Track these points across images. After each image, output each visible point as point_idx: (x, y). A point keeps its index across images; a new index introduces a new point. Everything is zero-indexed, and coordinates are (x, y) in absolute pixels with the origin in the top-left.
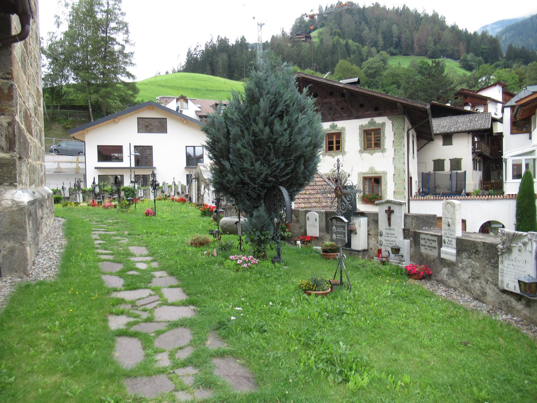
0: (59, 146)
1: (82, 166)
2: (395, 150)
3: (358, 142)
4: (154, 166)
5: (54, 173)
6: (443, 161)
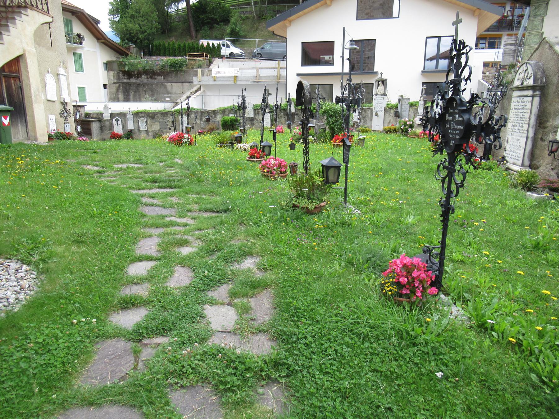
0: (262, 48)
1: (283, 72)
4: (375, 70)
5: (252, 83)
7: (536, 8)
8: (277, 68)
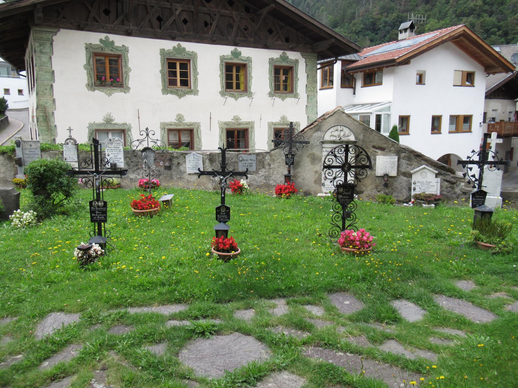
2: (308, 96)
3: (268, 81)
6: (236, 89)
7: (40, 45)
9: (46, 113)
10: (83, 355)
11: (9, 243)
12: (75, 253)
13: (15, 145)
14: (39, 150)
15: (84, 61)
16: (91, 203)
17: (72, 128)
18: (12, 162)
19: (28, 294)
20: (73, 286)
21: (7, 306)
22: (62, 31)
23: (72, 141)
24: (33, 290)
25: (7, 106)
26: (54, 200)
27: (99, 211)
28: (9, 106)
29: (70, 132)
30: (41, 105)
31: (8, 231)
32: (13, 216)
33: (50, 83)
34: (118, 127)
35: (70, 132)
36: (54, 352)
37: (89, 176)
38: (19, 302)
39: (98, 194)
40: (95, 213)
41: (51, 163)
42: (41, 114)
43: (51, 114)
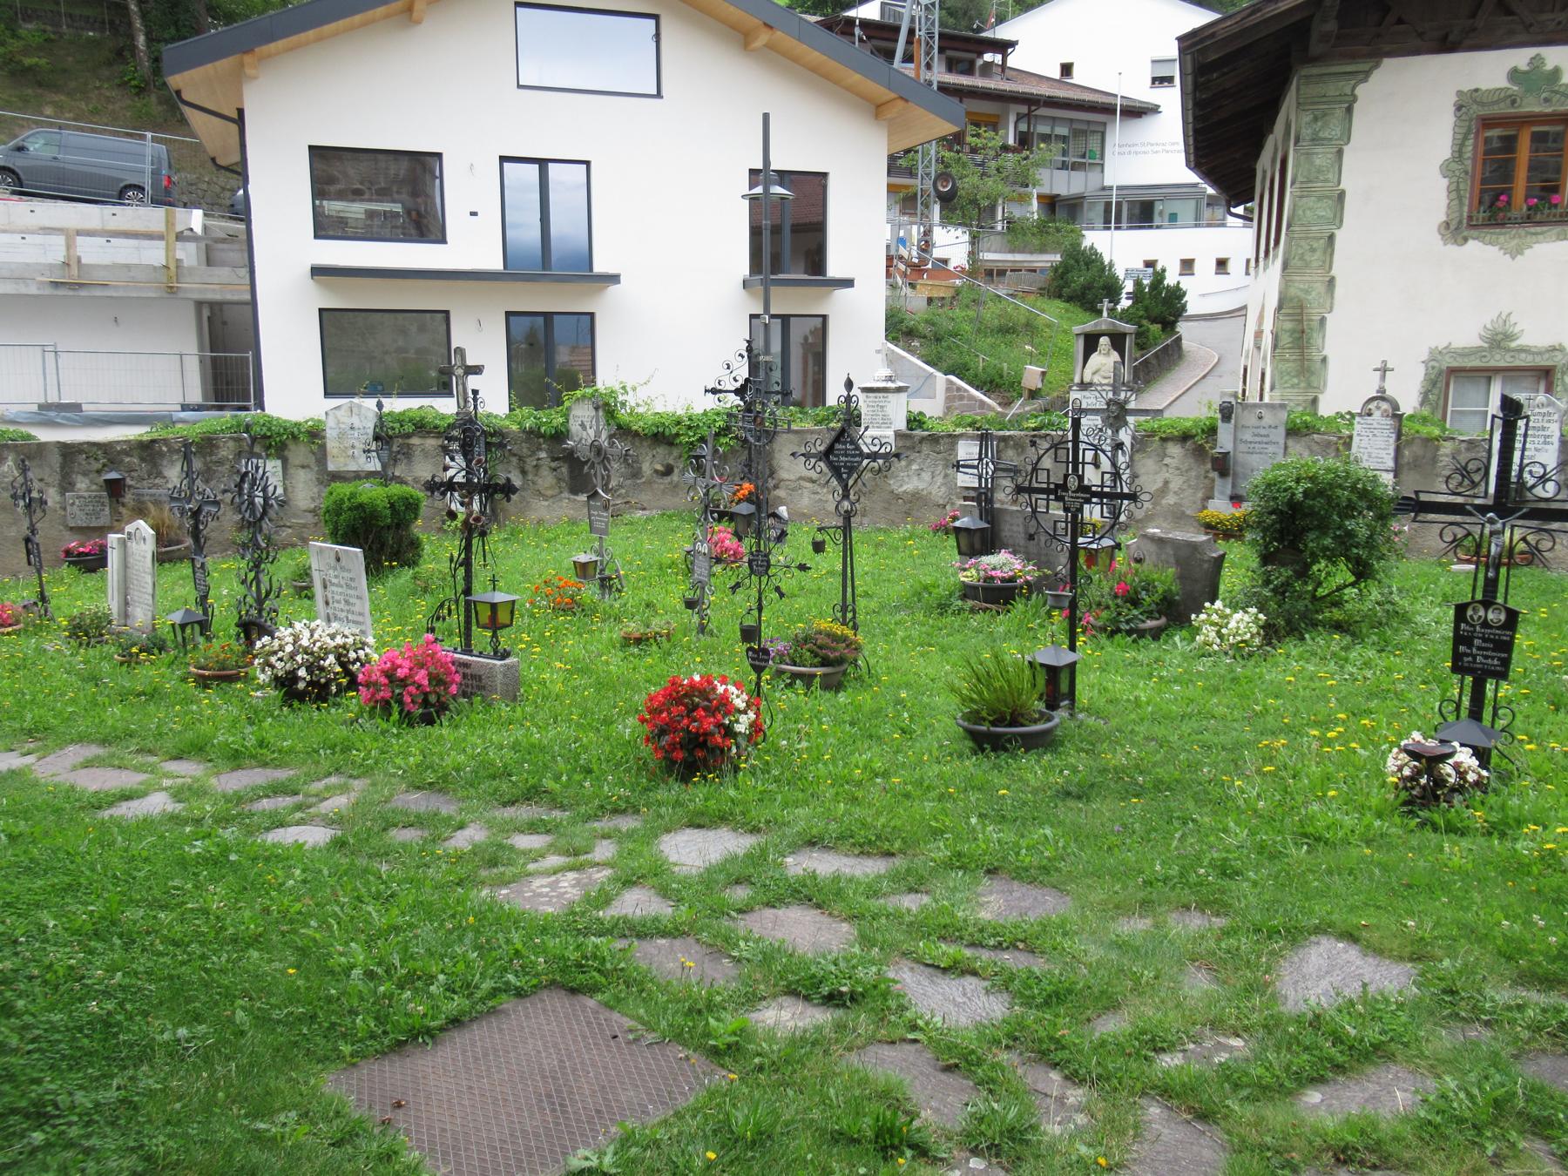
0: (20, 149)
5: (48, 291)
7: (1316, 119)
8: (160, 237)
9: (1301, 321)
10: (1438, 1119)
11: (1190, 692)
12: (1391, 764)
13: (1219, 416)
14: (1282, 431)
15: (1443, 148)
16: (1461, 610)
17: (1389, 366)
18: (1204, 463)
19: (1248, 857)
20: (1384, 868)
21: (1193, 878)
22: (1389, 63)
23: (1385, 406)
24: (1261, 848)
25: (1184, 308)
26: (1319, 584)
27: (1484, 640)
28: (1188, 307)
29: (1383, 378)
30: (1291, 300)
31: (1184, 656)
32: (1203, 617)
33: (1327, 229)
34: (1530, 358)
35: (1383, 378)
36: (1339, 1068)
37: (1468, 519)
38: (1224, 874)
39: (1491, 585)
40: (1470, 645)
41: (1328, 470)
42: (1288, 325)
43: (1315, 324)
